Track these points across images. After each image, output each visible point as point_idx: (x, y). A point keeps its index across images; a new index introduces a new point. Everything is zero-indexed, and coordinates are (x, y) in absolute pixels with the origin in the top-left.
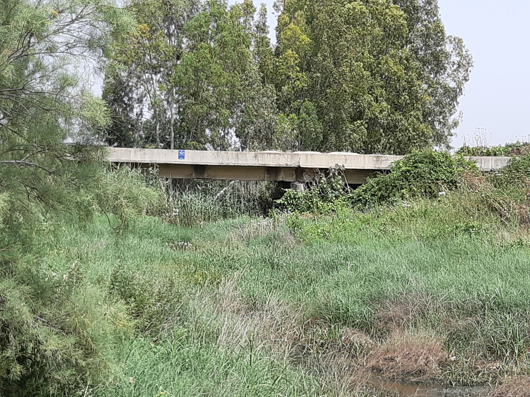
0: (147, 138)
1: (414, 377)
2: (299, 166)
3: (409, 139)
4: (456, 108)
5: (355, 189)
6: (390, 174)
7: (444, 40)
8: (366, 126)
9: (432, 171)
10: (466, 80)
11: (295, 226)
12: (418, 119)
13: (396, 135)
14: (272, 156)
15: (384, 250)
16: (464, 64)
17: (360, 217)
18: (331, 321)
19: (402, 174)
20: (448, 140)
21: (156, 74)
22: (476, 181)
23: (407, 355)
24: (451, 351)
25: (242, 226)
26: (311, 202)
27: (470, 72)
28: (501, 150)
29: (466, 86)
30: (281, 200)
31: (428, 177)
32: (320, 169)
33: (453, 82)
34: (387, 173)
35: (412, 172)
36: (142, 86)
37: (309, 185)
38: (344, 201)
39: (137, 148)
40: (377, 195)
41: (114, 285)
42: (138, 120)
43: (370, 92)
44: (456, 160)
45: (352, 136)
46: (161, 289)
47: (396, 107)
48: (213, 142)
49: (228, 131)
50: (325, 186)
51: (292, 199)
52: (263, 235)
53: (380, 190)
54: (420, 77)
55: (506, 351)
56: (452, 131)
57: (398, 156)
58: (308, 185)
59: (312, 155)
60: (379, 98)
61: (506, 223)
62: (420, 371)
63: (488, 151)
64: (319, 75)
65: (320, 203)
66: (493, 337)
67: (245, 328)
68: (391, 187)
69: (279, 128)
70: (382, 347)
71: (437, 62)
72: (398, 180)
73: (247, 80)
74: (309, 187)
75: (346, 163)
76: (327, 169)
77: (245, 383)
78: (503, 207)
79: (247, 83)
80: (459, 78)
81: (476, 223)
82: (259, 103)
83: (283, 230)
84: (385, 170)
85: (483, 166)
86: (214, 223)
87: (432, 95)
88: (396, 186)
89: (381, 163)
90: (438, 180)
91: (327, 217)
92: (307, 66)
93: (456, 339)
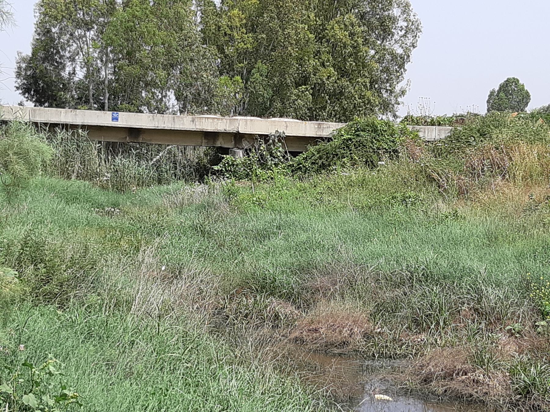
0: (80, 98)
1: (338, 348)
2: (238, 132)
3: (355, 106)
4: (404, 75)
5: (295, 157)
6: (331, 143)
7: (391, 5)
8: (311, 91)
9: (374, 140)
10: (414, 47)
11: (230, 193)
12: (365, 86)
13: (342, 102)
14: (210, 120)
15: (318, 220)
16: (412, 29)
17: (298, 185)
18: (257, 291)
19: (344, 142)
20: (395, 109)
21: (89, 30)
22: (417, 151)
23: (331, 326)
24: (377, 323)
25: (176, 192)
26: (250, 169)
27: (419, 37)
28: (446, 119)
29: (414, 53)
30: (219, 167)
31: (369, 145)
32: (261, 136)
33: (400, 49)
34: (329, 141)
35: (353, 140)
36: (74, 44)
37: (248, 151)
38: (284, 169)
39: (69, 108)
40: (317, 164)
41: (23, 250)
42: (70, 79)
43: (316, 57)
44: (399, 128)
45: (296, 103)
46: (75, 256)
47: (343, 73)
48: (148, 104)
49: (166, 94)
50: (264, 153)
51: (230, 165)
52: (197, 201)
53: (320, 158)
54: (366, 42)
55: (432, 323)
56: (399, 100)
57: (340, 124)
58: (247, 152)
59: (251, 120)
60: (326, 64)
61: (444, 194)
62: (344, 343)
63: (432, 120)
64: (264, 36)
65: (259, 171)
66: (419, 308)
67: (158, 296)
68: (332, 156)
69: (218, 92)
70: (307, 317)
71: (385, 28)
72: (339, 148)
73: (186, 40)
74: (248, 154)
75: (286, 129)
76: (267, 136)
77: (152, 352)
78: (441, 178)
79: (186, 43)
80: (406, 44)
81: (413, 194)
82: (198, 65)
83: (218, 197)
84: (326, 138)
85: (426, 136)
86: (148, 189)
87: (379, 61)
88: (337, 155)
89: (323, 130)
90: (379, 149)
91: (266, 185)
92: (252, 27)
93: (383, 311)
